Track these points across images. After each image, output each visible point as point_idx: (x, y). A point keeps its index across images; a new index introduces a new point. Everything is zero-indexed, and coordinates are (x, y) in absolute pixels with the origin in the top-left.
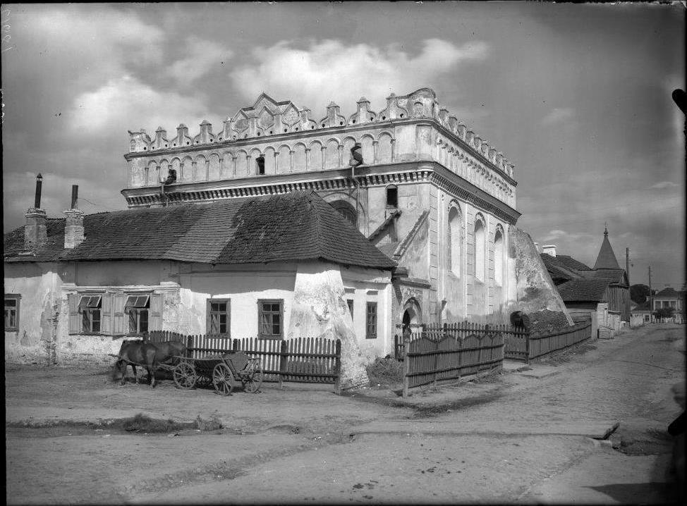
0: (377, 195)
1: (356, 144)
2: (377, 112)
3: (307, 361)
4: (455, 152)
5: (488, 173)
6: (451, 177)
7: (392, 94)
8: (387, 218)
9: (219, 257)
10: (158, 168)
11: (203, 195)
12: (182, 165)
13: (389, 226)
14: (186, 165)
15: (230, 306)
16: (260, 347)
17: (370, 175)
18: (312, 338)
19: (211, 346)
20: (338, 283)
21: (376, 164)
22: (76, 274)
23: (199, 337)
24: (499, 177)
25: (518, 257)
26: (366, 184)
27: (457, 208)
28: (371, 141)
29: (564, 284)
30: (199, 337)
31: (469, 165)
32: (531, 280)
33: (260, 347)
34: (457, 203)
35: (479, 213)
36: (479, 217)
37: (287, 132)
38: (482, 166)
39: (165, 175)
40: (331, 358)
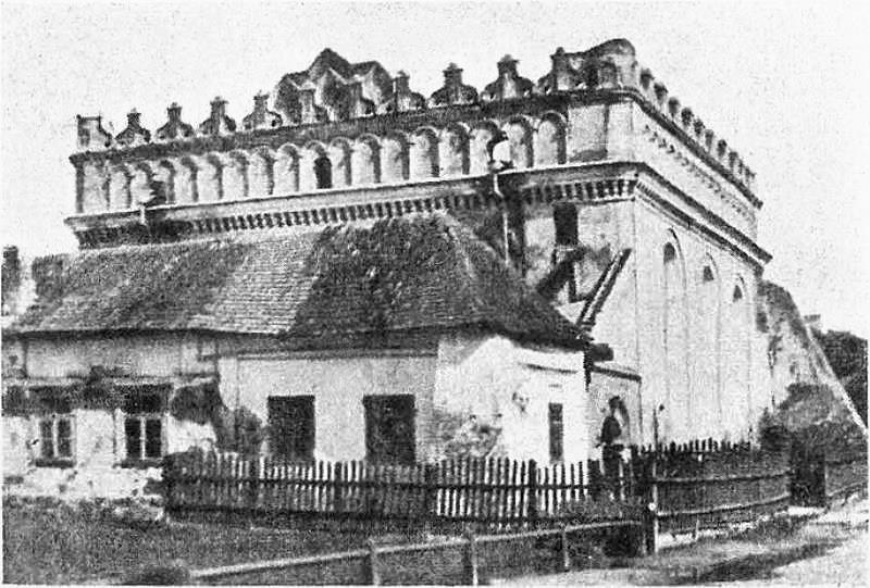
0: (540, 230)
2: (535, 80)
3: (377, 470)
4: (668, 147)
8: (559, 261)
9: (295, 325)
13: (562, 274)
16: (563, 477)
20: (708, 120)
25: (772, 332)
31: (691, 171)
32: (796, 371)
33: (563, 477)
40: (463, 491)
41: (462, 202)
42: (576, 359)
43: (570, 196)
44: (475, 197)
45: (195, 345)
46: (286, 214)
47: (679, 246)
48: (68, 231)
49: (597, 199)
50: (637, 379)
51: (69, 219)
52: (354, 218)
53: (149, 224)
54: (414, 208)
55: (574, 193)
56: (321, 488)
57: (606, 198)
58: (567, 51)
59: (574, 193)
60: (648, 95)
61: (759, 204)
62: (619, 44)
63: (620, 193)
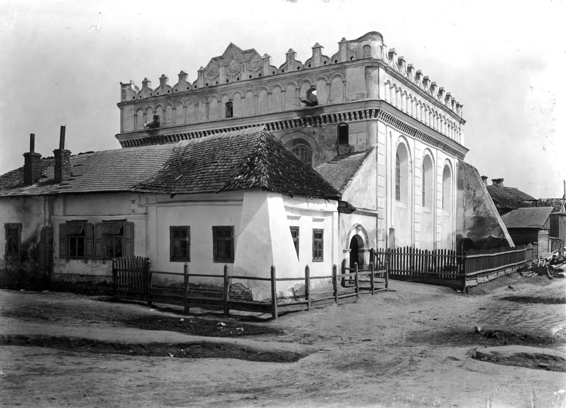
1: (312, 86)
5: (436, 112)
6: (399, 114)
7: (344, 39)
10: (145, 114)
11: (178, 137)
12: (164, 111)
14: (167, 110)
15: (189, 232)
17: (324, 114)
18: (442, 250)
19: (120, 267)
21: (329, 104)
22: (65, 205)
23: (399, 249)
24: (448, 116)
25: (466, 189)
26: (320, 123)
27: (406, 144)
28: (324, 83)
29: (509, 213)
30: (399, 249)
32: (477, 209)
34: (430, 150)
35: (427, 149)
36: (428, 152)
37: (252, 78)
38: (431, 106)
39: (150, 120)
41: (293, 124)
42: (333, 206)
43: (345, 119)
44: (299, 120)
45: (62, 200)
46: (173, 136)
47: (408, 145)
48: (117, 141)
49: (364, 119)
50: (376, 215)
51: (117, 135)
52: (201, 136)
53: (158, 137)
54: (203, 135)
55: (347, 117)
56: (383, 255)
57: (363, 120)
58: (348, 39)
59: (347, 117)
60: (393, 64)
61: (463, 122)
62: (373, 34)
63: (370, 117)
